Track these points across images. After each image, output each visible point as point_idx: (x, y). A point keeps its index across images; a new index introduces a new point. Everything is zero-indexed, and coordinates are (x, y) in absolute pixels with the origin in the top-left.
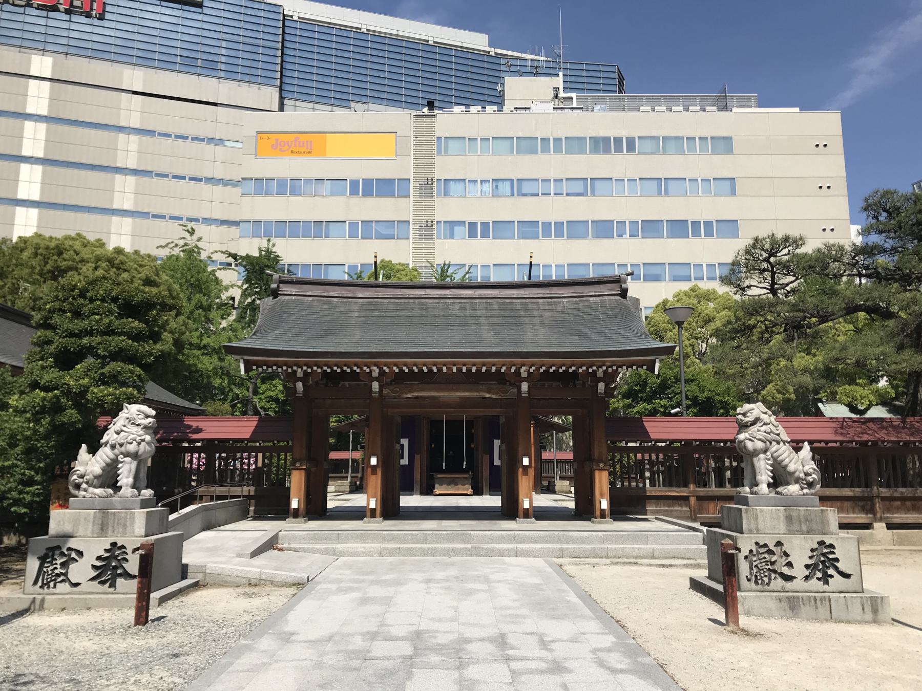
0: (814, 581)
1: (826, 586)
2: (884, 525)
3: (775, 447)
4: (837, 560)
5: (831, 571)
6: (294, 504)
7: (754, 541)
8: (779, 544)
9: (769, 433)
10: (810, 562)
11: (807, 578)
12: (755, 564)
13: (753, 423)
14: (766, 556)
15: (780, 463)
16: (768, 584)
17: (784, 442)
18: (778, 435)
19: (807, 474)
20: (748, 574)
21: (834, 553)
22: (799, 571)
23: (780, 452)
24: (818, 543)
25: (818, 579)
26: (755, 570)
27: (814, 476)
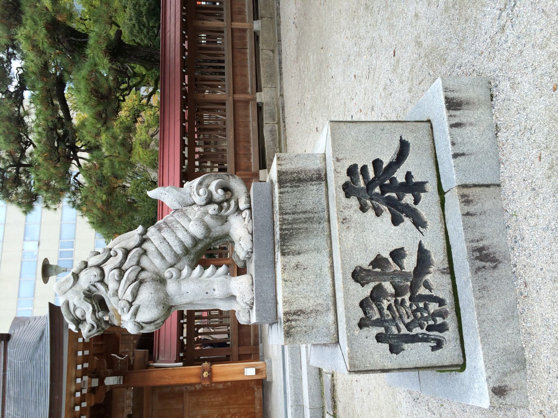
0: (420, 208)
1: (428, 187)
2: (258, 94)
3: (153, 262)
4: (377, 163)
5: (400, 176)
6: (250, 372)
7: (357, 331)
8: (358, 275)
9: (121, 276)
10: (387, 216)
11: (419, 223)
12: (404, 331)
13: (101, 304)
14: (385, 304)
15: (187, 251)
16: (441, 302)
17: (143, 241)
18: (127, 252)
19: (210, 201)
20: (427, 346)
21: (364, 168)
22: (405, 236)
23: (163, 249)
24: (348, 196)
25: (416, 202)
26: (417, 330)
27: (212, 188)
